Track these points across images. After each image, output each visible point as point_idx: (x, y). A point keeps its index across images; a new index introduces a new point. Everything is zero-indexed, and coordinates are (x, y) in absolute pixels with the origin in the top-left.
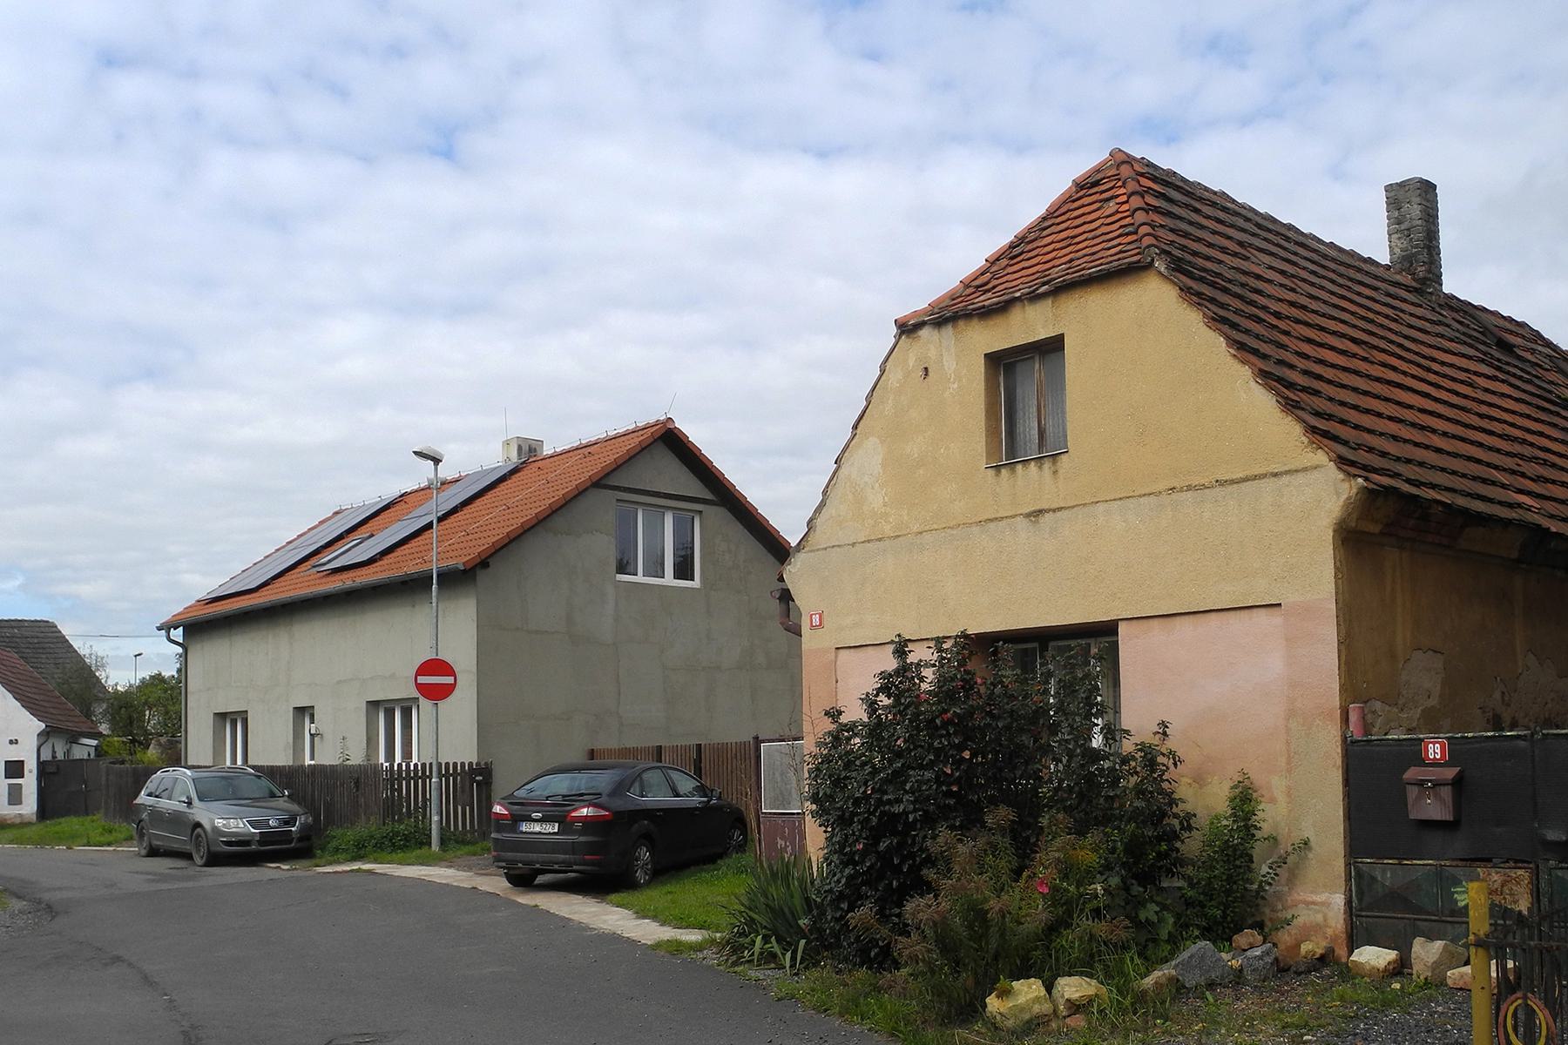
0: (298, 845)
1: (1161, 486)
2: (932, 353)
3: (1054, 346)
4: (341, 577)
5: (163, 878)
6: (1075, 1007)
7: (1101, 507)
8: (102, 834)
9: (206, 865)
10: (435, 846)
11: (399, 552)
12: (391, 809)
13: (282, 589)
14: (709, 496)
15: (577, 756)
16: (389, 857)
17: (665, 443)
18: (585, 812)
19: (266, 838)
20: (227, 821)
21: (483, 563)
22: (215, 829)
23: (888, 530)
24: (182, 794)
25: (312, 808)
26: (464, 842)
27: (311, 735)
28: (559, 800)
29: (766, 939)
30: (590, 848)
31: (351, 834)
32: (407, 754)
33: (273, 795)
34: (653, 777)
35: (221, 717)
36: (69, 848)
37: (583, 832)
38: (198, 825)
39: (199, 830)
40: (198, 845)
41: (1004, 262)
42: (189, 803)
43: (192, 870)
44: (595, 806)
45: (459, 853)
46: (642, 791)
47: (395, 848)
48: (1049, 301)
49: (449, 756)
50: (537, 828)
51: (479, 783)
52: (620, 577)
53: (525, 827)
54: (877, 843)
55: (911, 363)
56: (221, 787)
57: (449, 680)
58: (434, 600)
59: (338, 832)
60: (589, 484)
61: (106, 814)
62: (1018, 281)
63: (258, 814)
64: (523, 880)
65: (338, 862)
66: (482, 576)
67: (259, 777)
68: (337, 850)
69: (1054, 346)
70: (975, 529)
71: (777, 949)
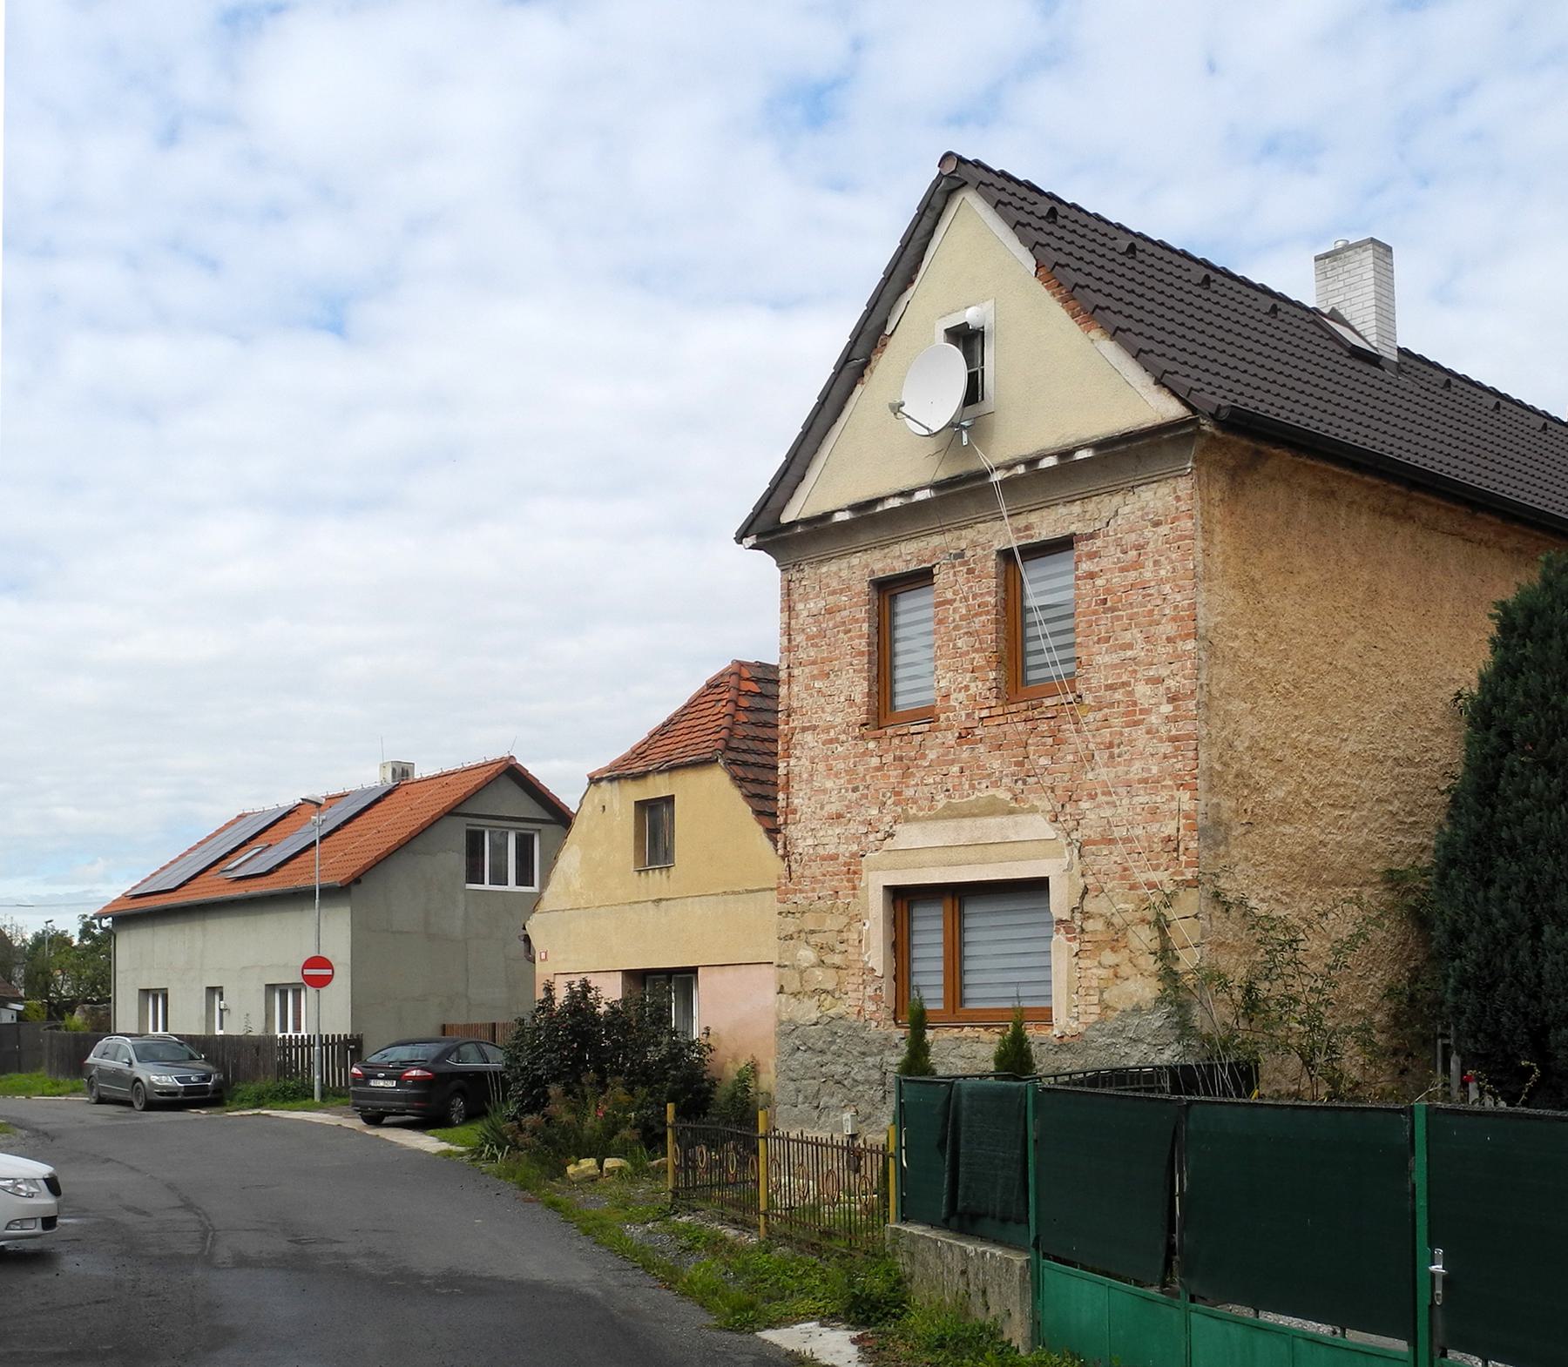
0: (213, 1096)
1: (720, 890)
2: (607, 797)
3: (669, 800)
4: (245, 885)
5: (116, 1118)
6: (611, 1172)
7: (690, 899)
8: (51, 1088)
9: (143, 1110)
10: (317, 1098)
11: (291, 865)
12: (284, 1070)
13: (195, 891)
14: (546, 816)
15: (431, 1030)
16: (282, 1106)
17: (508, 775)
18: (414, 1073)
19: (189, 1090)
20: (161, 1078)
21: (357, 880)
22: (151, 1083)
23: (583, 903)
24: (123, 1057)
25: (222, 1067)
26: (340, 1096)
27: (221, 1010)
28: (397, 1065)
29: (491, 1146)
30: (418, 1098)
31: (252, 1089)
32: (297, 1028)
33: (192, 1058)
34: (469, 1049)
35: (145, 993)
36: (28, 1098)
37: (413, 1087)
38: (138, 1080)
39: (138, 1083)
40: (137, 1096)
41: (657, 737)
42: (130, 1064)
43: (134, 1114)
44: (422, 1069)
45: (334, 1104)
46: (459, 1058)
47: (286, 1099)
48: (667, 774)
49: (329, 1030)
50: (381, 1083)
51: (352, 1050)
52: (470, 886)
53: (373, 1083)
54: (532, 1091)
55: (596, 801)
56: (147, 1053)
57: (327, 972)
58: (317, 906)
59: (242, 1086)
60: (442, 814)
61: (50, 1071)
62: (656, 757)
63: (184, 1073)
64: (374, 1120)
65: (243, 1109)
66: (354, 889)
67: (181, 1044)
68: (242, 1100)
69: (669, 800)
70: (627, 907)
71: (496, 1151)
